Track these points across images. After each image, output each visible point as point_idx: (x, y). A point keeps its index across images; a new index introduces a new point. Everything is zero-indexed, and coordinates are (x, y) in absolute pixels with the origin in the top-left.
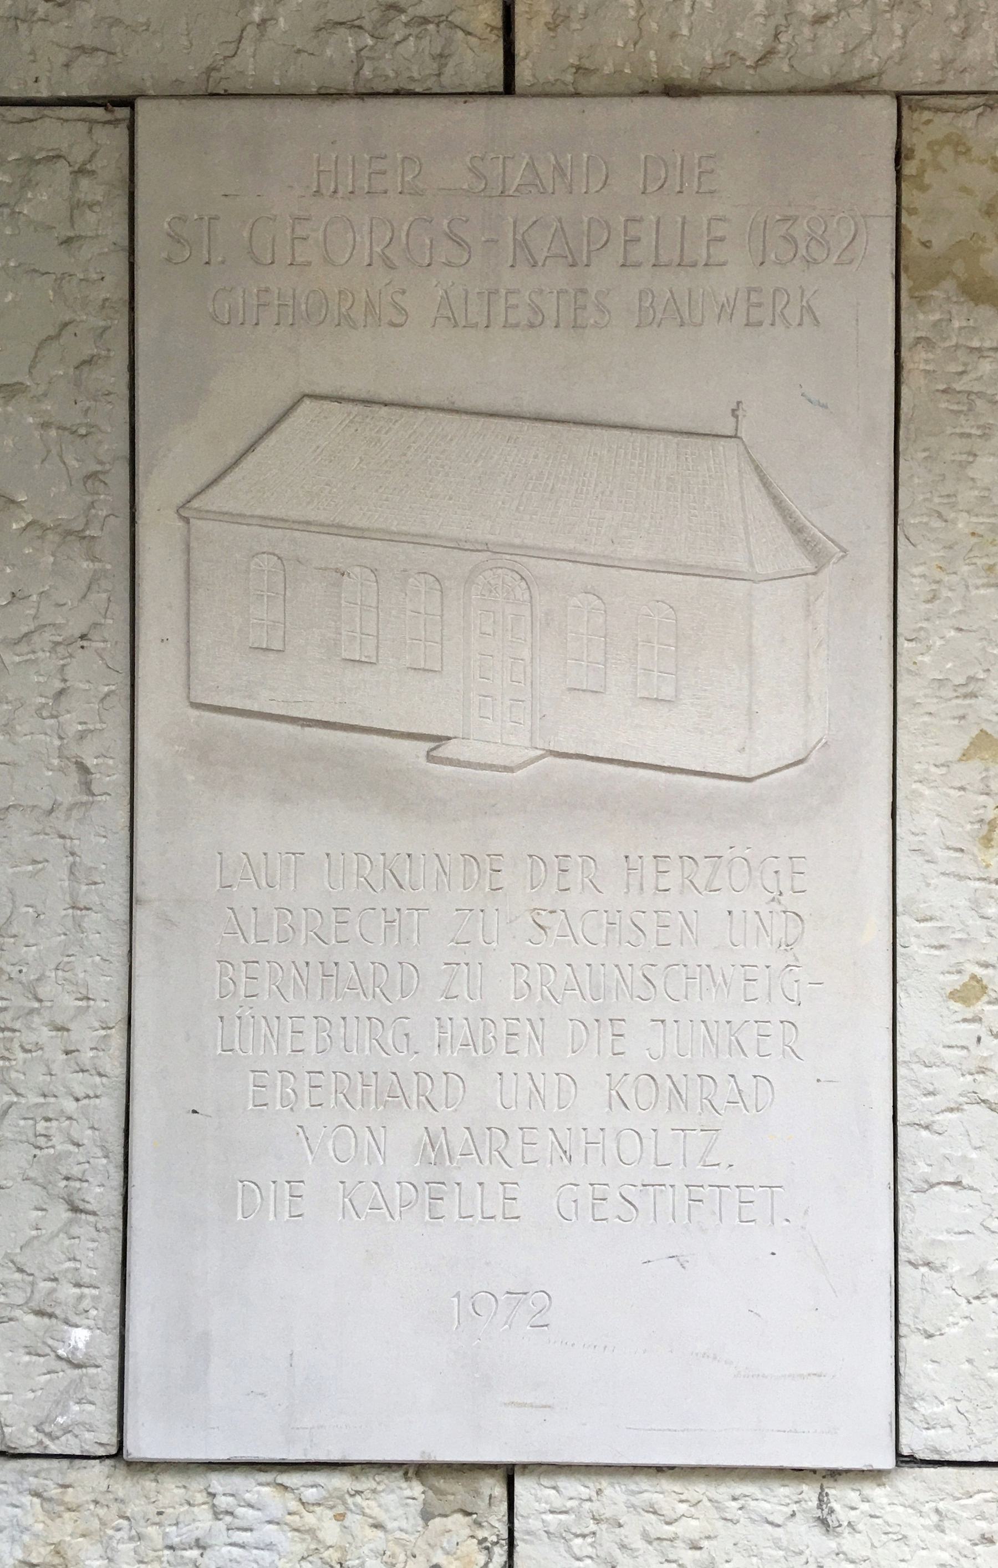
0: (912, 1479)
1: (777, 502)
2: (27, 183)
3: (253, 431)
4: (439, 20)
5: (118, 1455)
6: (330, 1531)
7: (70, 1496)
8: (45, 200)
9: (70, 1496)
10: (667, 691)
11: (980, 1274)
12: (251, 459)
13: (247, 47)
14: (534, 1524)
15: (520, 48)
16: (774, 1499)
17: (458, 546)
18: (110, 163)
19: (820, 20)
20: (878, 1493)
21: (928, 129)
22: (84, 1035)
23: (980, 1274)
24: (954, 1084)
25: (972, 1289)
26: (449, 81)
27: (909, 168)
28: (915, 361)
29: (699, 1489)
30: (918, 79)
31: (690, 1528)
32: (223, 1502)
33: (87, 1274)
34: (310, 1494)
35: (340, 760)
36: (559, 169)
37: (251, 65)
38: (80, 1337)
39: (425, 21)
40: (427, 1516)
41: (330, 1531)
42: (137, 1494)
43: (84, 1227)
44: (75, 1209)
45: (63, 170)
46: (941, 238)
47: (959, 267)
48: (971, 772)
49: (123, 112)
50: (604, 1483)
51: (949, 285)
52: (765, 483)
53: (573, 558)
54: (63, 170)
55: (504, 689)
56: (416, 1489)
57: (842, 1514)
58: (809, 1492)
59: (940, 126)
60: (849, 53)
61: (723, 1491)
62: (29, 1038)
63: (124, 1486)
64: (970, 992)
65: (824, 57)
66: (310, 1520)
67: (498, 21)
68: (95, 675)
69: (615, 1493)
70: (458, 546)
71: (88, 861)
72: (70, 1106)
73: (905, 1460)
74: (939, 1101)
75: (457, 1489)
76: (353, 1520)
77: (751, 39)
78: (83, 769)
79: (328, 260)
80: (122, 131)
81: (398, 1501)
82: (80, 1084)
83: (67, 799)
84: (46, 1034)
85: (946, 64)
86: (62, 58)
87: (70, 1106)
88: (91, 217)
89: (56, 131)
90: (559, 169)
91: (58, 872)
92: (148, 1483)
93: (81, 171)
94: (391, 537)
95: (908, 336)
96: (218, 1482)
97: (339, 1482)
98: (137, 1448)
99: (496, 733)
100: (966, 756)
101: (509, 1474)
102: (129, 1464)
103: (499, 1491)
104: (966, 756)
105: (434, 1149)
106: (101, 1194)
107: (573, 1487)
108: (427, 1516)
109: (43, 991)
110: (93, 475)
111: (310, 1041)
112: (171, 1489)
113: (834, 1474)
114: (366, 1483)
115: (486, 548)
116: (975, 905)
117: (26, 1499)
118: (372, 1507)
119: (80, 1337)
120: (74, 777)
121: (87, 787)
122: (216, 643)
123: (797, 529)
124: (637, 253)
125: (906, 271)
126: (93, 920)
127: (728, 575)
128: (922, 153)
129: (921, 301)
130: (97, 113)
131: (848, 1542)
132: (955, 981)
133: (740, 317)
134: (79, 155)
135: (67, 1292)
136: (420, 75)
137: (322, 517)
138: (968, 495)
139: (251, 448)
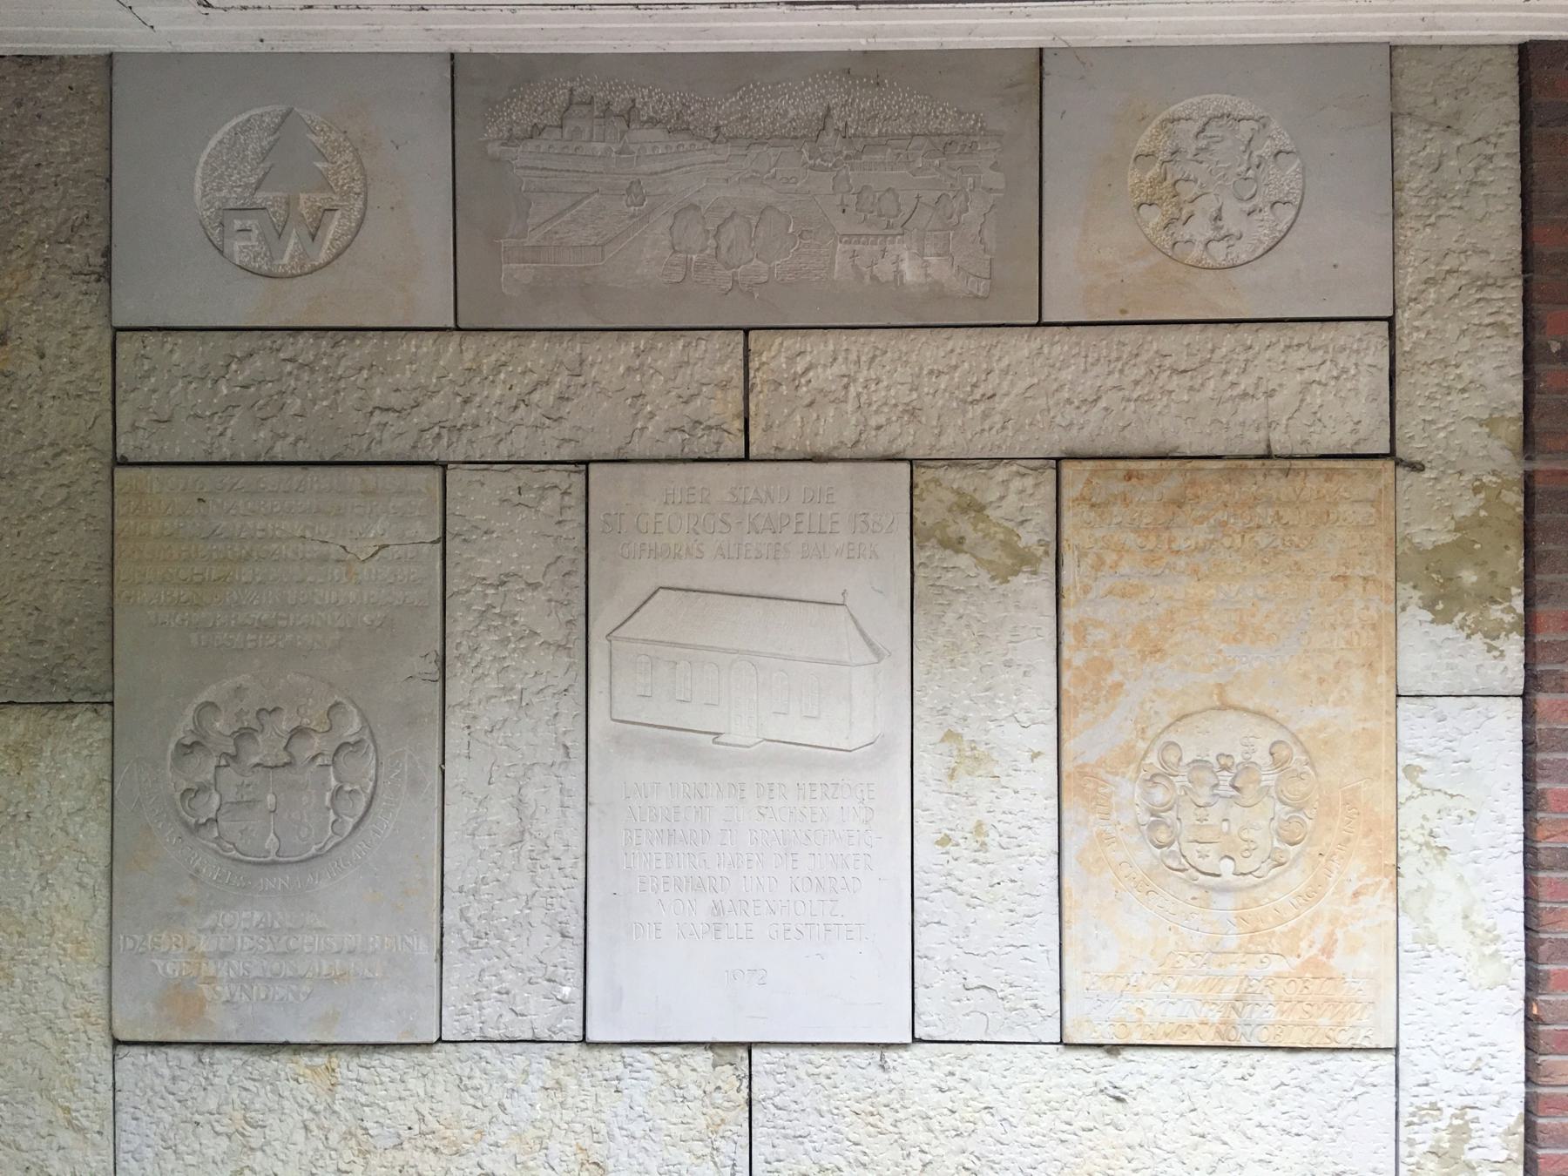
0: (919, 1049)
1: (863, 634)
2: (542, 498)
3: (636, 605)
4: (718, 427)
5: (747, 331)
6: (673, 1072)
7: (562, 1059)
8: (551, 502)
9: (562, 1059)
10: (815, 713)
11: (949, 961)
12: (637, 615)
13: (636, 439)
14: (760, 1068)
15: (752, 440)
16: (862, 1057)
17: (725, 651)
18: (578, 490)
19: (879, 428)
20: (906, 1054)
21: (923, 476)
22: (567, 861)
23: (949, 961)
24: (937, 881)
25: (945, 967)
26: (721, 455)
27: (916, 492)
28: (919, 572)
29: (830, 1053)
30: (920, 454)
31: (827, 1070)
32: (628, 1060)
33: (570, 964)
34: (665, 1057)
35: (674, 742)
36: (768, 493)
37: (638, 449)
38: (566, 990)
39: (710, 428)
40: (714, 1066)
41: (673, 1072)
42: (591, 1057)
43: (568, 943)
44: (563, 936)
45: (557, 493)
46: (930, 521)
47: (938, 533)
48: (944, 747)
49: (583, 467)
50: (789, 1051)
51: (934, 541)
52: (856, 622)
53: (774, 656)
54: (557, 493)
55: (747, 715)
56: (710, 1054)
57: (890, 1063)
58: (877, 1054)
59: (930, 474)
60: (891, 442)
61: (840, 1054)
62: (544, 863)
63: (586, 1054)
64: (945, 841)
65: (880, 445)
66: (665, 1068)
67: (742, 427)
68: (571, 707)
69: (795, 1055)
70: (725, 651)
71: (567, 786)
72: (562, 892)
73: (915, 1040)
74: (932, 888)
75: (727, 1054)
76: (683, 1067)
77: (849, 434)
78: (566, 747)
79: (671, 531)
80: (583, 476)
81: (702, 1059)
82: (566, 882)
83: (559, 760)
84: (551, 861)
85: (932, 447)
86: (556, 443)
87: (562, 892)
88: (569, 512)
89: (553, 476)
90: (768, 493)
91: (555, 792)
92: (596, 1053)
93: (565, 493)
94: (695, 647)
95: (916, 562)
96: (625, 1051)
97: (677, 1051)
98: (591, 1037)
99: (741, 732)
100: (942, 741)
101: (749, 1047)
102: (588, 1044)
103: (746, 1055)
104: (942, 741)
105: (717, 909)
106: (576, 930)
107: (777, 1053)
108: (714, 1066)
109: (550, 843)
110: (570, 622)
111: (663, 864)
112: (606, 1055)
113: (887, 1046)
114: (689, 1052)
115: (738, 651)
116: (947, 804)
117: (544, 1060)
118: (691, 1062)
119: (566, 990)
120: (562, 751)
121: (568, 755)
122: (624, 694)
123: (870, 644)
124: (801, 528)
125: (1094, 472)
126: (569, 812)
127: (839, 663)
128: (922, 485)
129: (922, 548)
130: (572, 467)
131: (893, 1075)
132: (939, 836)
133: (845, 555)
134: (564, 486)
135: (561, 971)
136: (708, 452)
137: (666, 639)
138: (943, 629)
139: (637, 610)
